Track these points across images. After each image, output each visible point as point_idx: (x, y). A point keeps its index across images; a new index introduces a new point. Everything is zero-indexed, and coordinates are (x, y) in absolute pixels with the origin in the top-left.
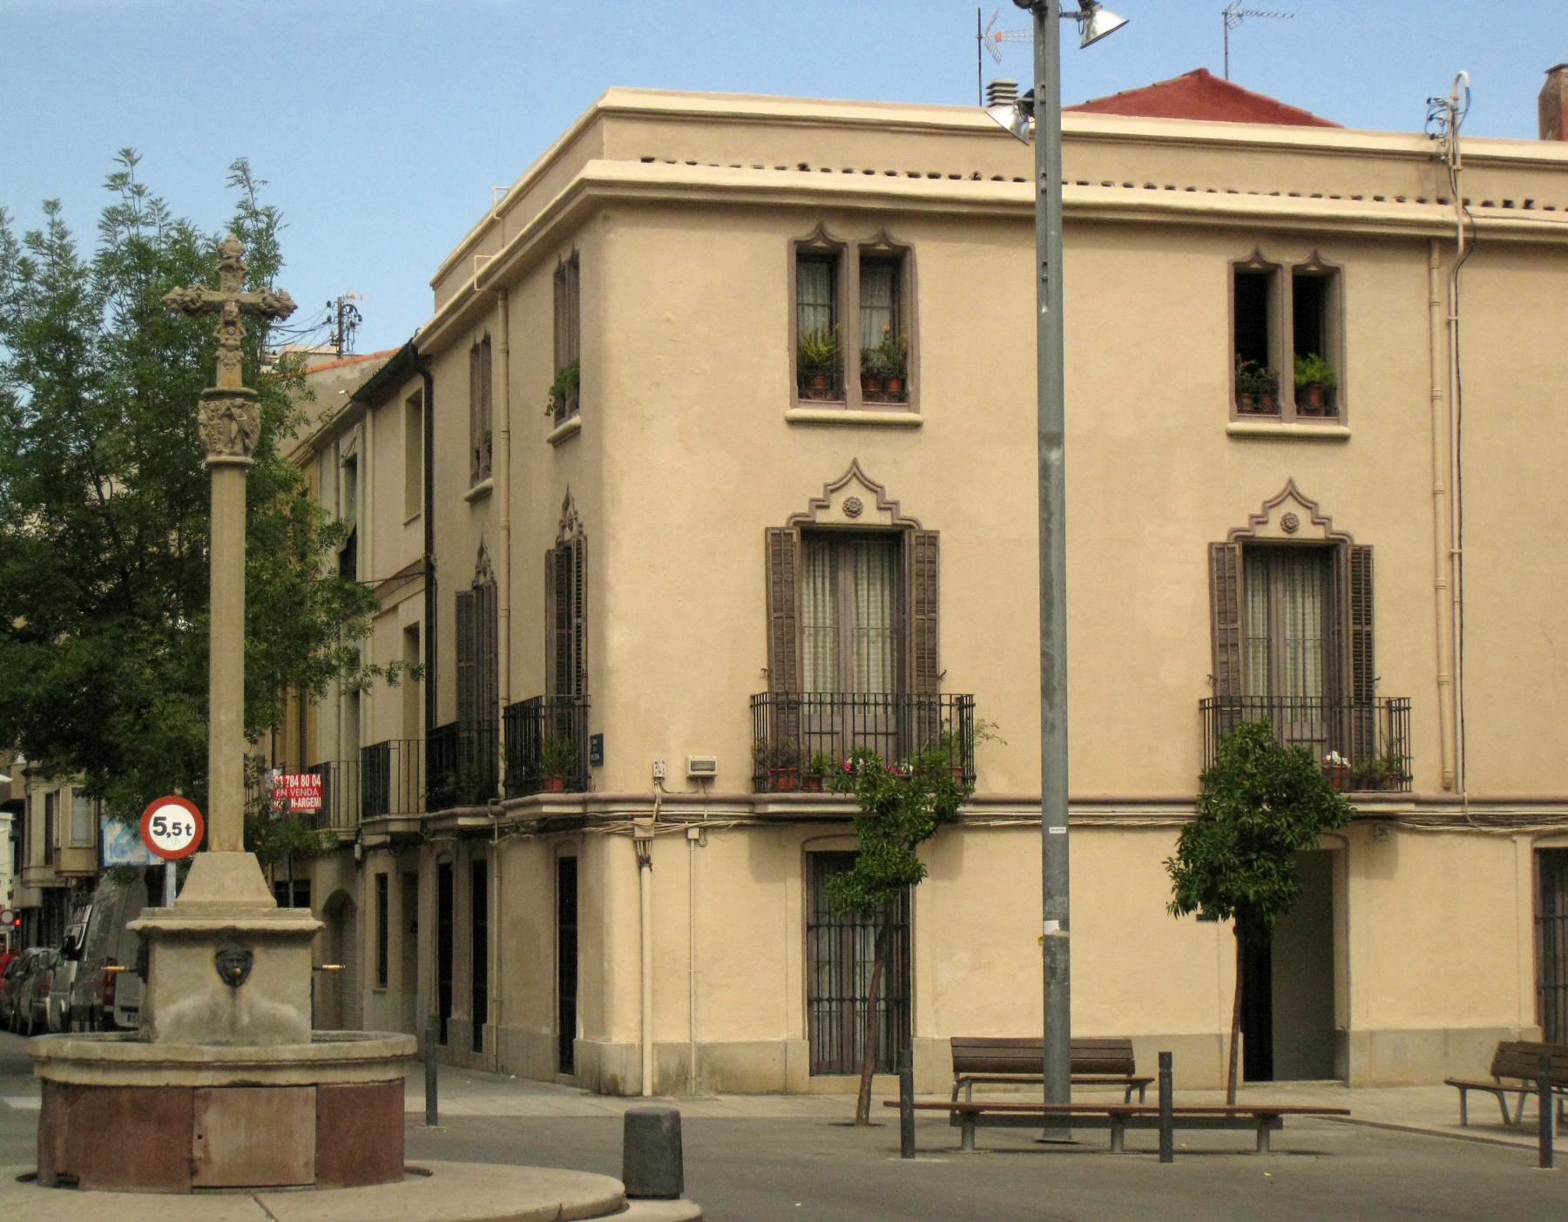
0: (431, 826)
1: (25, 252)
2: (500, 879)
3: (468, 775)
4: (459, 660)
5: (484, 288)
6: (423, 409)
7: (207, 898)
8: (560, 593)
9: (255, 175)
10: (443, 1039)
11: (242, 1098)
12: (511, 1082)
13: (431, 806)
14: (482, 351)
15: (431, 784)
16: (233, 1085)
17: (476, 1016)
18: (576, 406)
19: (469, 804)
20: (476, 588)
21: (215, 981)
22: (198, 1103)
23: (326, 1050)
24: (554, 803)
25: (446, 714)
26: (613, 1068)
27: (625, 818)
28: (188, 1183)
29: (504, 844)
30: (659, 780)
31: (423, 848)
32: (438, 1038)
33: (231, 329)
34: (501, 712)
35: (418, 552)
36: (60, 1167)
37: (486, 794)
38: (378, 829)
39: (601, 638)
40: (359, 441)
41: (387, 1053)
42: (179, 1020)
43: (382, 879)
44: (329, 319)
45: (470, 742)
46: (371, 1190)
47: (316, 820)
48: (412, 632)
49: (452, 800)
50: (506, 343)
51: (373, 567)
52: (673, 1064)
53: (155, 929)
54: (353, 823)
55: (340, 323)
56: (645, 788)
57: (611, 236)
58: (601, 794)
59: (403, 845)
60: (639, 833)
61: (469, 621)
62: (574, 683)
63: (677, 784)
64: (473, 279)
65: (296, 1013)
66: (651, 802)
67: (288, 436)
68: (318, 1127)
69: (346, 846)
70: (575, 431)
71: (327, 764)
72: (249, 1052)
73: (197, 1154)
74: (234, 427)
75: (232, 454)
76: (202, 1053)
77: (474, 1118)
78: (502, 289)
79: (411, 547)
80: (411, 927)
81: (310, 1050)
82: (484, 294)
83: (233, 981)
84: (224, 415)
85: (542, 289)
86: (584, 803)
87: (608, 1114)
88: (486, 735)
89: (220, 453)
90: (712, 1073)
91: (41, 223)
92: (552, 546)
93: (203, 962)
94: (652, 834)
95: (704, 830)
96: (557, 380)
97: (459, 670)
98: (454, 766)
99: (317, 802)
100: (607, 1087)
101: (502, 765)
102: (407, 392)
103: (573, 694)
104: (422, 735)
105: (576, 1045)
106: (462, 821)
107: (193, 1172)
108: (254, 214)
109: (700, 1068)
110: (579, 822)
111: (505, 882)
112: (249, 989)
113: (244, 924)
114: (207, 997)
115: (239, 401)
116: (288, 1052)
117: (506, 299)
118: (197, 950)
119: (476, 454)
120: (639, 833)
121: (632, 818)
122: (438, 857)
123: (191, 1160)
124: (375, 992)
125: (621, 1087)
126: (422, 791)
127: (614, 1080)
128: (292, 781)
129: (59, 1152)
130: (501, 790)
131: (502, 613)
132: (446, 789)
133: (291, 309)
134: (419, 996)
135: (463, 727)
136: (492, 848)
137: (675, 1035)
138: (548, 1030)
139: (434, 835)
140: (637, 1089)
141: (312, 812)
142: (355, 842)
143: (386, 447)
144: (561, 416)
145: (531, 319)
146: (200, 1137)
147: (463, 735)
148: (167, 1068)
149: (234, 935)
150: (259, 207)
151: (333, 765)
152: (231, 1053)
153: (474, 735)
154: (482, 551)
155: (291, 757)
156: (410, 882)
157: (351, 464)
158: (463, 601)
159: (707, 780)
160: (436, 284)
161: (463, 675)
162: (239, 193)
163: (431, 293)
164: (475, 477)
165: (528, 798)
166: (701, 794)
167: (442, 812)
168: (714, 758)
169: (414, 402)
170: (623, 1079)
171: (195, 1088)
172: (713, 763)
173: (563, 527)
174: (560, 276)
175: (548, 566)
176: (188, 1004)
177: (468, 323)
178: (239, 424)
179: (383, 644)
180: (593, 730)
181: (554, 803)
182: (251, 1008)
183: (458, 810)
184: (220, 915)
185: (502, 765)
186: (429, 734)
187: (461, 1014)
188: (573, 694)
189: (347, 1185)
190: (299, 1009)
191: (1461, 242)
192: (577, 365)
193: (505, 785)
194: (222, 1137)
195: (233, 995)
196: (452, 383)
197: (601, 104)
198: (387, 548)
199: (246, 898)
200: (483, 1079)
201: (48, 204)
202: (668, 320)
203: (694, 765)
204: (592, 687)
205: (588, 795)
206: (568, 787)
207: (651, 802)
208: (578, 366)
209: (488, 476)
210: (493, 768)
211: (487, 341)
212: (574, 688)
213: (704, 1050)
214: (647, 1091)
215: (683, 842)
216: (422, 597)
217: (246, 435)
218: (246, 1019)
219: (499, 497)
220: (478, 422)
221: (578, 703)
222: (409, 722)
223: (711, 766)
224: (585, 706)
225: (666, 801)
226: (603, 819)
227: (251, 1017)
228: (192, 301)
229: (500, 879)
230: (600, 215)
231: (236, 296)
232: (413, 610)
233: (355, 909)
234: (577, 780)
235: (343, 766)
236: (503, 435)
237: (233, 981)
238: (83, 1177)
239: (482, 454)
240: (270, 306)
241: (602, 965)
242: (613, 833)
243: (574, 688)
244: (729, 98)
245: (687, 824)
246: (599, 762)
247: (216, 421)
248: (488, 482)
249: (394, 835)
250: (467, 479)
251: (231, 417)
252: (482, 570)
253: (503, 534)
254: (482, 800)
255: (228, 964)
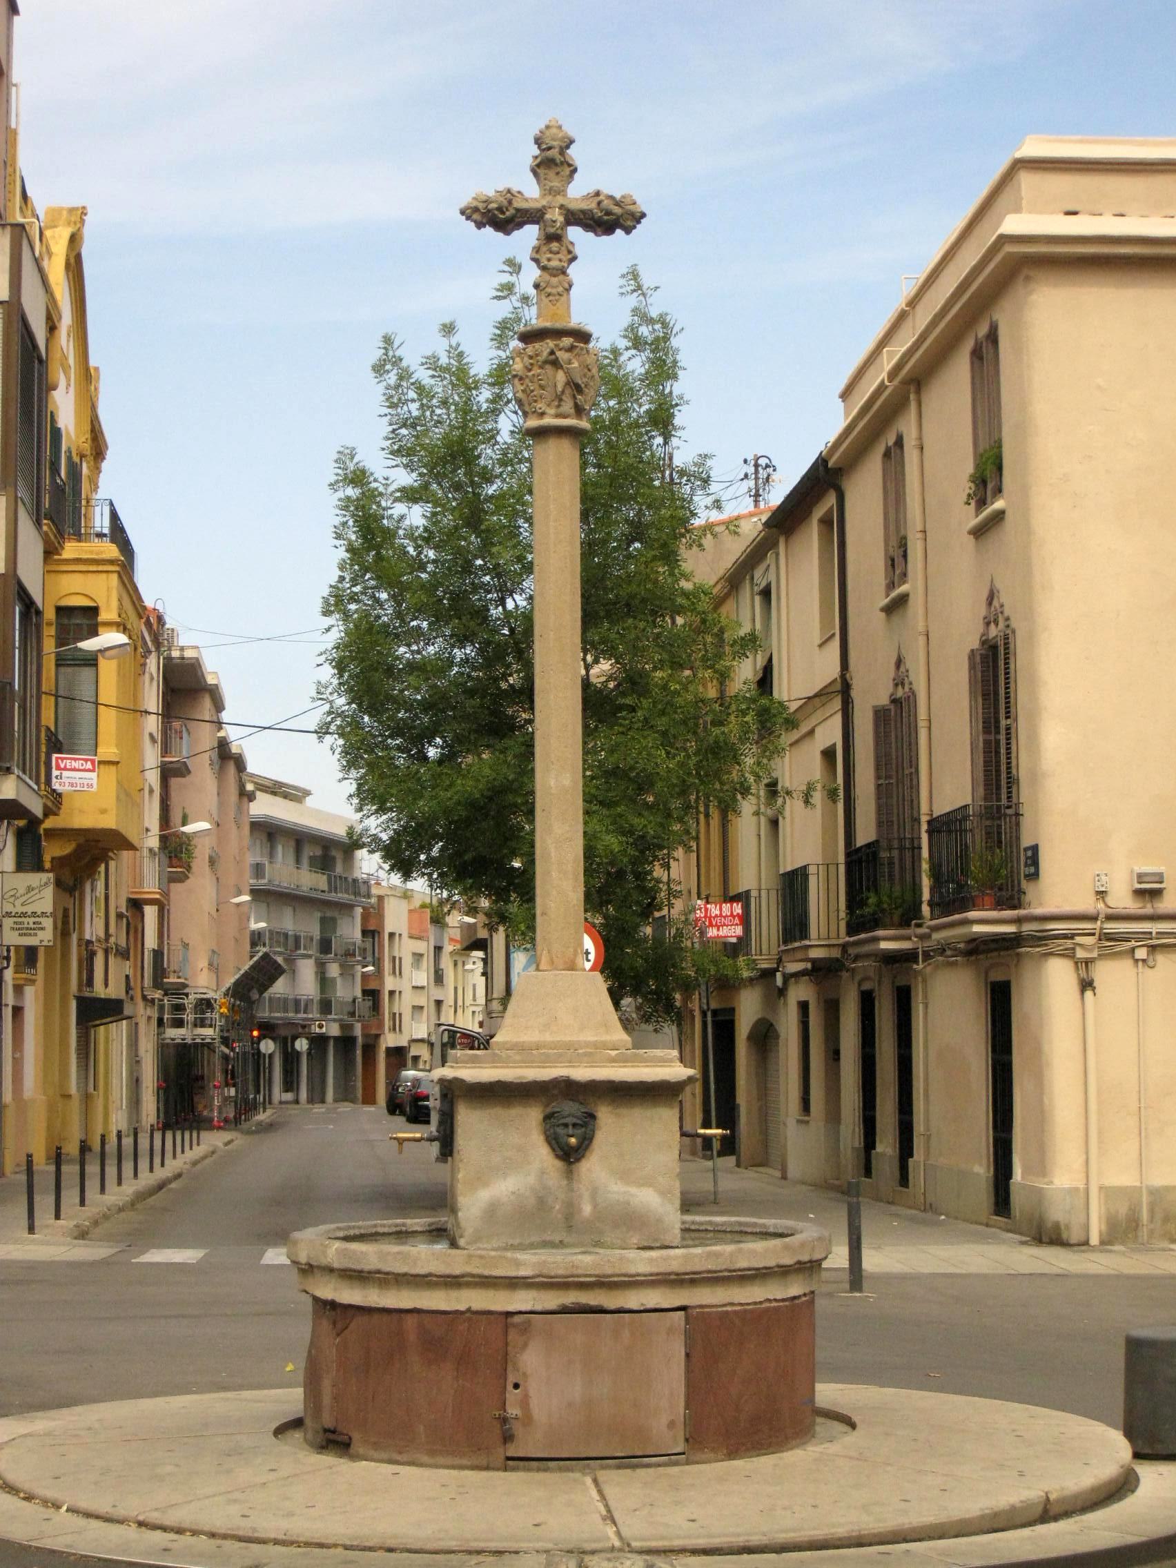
0: (852, 951)
1: (424, 376)
2: (926, 1006)
3: (890, 897)
4: (878, 777)
5: (896, 382)
6: (835, 527)
7: (530, 1037)
8: (985, 696)
9: (647, 282)
10: (868, 1172)
11: (576, 1329)
12: (941, 1223)
13: (852, 929)
14: (894, 455)
15: (851, 906)
16: (564, 1310)
17: (901, 1149)
18: (999, 490)
19: (892, 926)
20: (894, 701)
21: (542, 1154)
22: (513, 1335)
23: (697, 1257)
24: (985, 922)
25: (866, 833)
26: (1056, 1213)
27: (1065, 937)
28: (500, 1453)
29: (929, 969)
30: (1101, 894)
31: (845, 975)
32: (863, 1171)
33: (554, 246)
34: (924, 827)
35: (834, 671)
36: (328, 1421)
37: (909, 916)
38: (799, 955)
39: (1034, 737)
40: (773, 569)
41: (788, 1260)
42: (492, 1211)
43: (804, 1007)
44: (746, 476)
45: (891, 864)
46: (764, 1463)
47: (735, 949)
48: (829, 754)
49: (875, 922)
50: (920, 438)
51: (791, 688)
52: (1123, 1210)
53: (457, 1081)
54: (774, 951)
55: (757, 479)
56: (1084, 903)
57: (1034, 297)
58: (1038, 911)
59: (822, 972)
60: (1080, 954)
61: (887, 735)
62: (1004, 791)
63: (1122, 899)
64: (884, 375)
65: (656, 1199)
66: (1093, 918)
67: (695, 548)
68: (688, 1371)
69: (768, 974)
70: (999, 516)
71: (748, 892)
72: (585, 1262)
73: (513, 1411)
74: (561, 377)
75: (557, 416)
76: (518, 1264)
77: (903, 1278)
78: (914, 381)
79: (827, 667)
80: (834, 1054)
81: (677, 1259)
82: (896, 388)
83: (570, 1155)
84: (546, 362)
85: (960, 371)
86: (1018, 921)
87: (1055, 1271)
88: (908, 854)
89: (542, 414)
90: (1166, 1219)
91: (440, 347)
92: (976, 645)
93: (525, 1128)
94: (1095, 954)
95: (1153, 949)
96: (977, 466)
97: (878, 786)
98: (876, 888)
99: (739, 931)
100: (1048, 1235)
101: (926, 883)
102: (819, 512)
103: (1004, 802)
104: (841, 858)
105: (1012, 1188)
106: (884, 945)
107: (508, 1438)
108: (651, 321)
109: (1152, 1212)
110: (1008, 944)
111: (930, 1010)
112: (593, 1167)
113: (581, 1074)
114: (531, 1180)
115: (567, 341)
116: (642, 1263)
117: (918, 392)
118: (515, 1111)
119: (892, 563)
120: (1080, 954)
121: (1072, 937)
122: (859, 985)
123: (504, 1420)
124: (798, 1121)
125: (1065, 1236)
126: (842, 915)
127: (1057, 1226)
128: (714, 910)
129: (327, 1400)
130: (926, 909)
131: (922, 724)
132: (867, 910)
133: (639, 217)
134: (842, 1127)
135: (884, 844)
136: (916, 972)
137: (1126, 1179)
138: (982, 1170)
139: (854, 961)
140: (1083, 1239)
141: (734, 940)
142: (777, 970)
143: (800, 573)
144: (982, 503)
145: (942, 432)
146: (516, 1386)
147: (884, 854)
148: (468, 1285)
149: (568, 1089)
150: (654, 313)
151: (754, 894)
152: (559, 1261)
153: (895, 853)
154: (899, 662)
155: (715, 888)
156: (832, 1009)
157: (766, 593)
158: (881, 716)
159: (1155, 894)
160: (845, 395)
161: (882, 792)
162: (633, 300)
163: (840, 404)
164: (891, 586)
165: (957, 917)
166: (1148, 910)
167: (863, 936)
168: (1162, 869)
169: (826, 522)
170: (1068, 1227)
171: (509, 1314)
172: (1161, 875)
173: (988, 624)
174: (977, 355)
175: (972, 667)
176: (506, 1188)
177: (879, 425)
178: (567, 373)
179: (799, 766)
180: (1026, 842)
181: (985, 922)
182: (594, 1193)
183: (880, 933)
184: (546, 1061)
185: (926, 883)
186: (848, 855)
187: (886, 1146)
188: (1004, 802)
189: (732, 1454)
190: (663, 1193)
191: (708, 1131)
192: (998, 445)
193: (930, 904)
194: (547, 1387)
195: (569, 1174)
196: (864, 496)
197: (1018, 155)
198: (803, 668)
199: (589, 1036)
200: (912, 1219)
201: (444, 326)
202: (1099, 387)
203: (1141, 877)
204: (1025, 793)
205: (1022, 912)
206: (1000, 904)
207: (1093, 918)
208: (1000, 447)
209: (904, 583)
210: (916, 888)
211: (899, 442)
212: (1004, 796)
213: (1155, 1193)
214: (1094, 1240)
215: (1130, 962)
216: (838, 719)
217: (578, 389)
218: (587, 1209)
219: (916, 605)
220: (892, 527)
221: (1009, 811)
222: (828, 843)
223: (1160, 878)
224: (1018, 815)
225: (1110, 918)
226: (1041, 939)
227: (595, 1206)
228: (500, 209)
229: (926, 1006)
230: (1022, 277)
231: (560, 200)
232: (830, 733)
233: (777, 1037)
234: (1009, 896)
235: (764, 893)
236: (920, 535)
237: (570, 1155)
238: (356, 1436)
239: (897, 562)
240: (608, 213)
241: (1041, 1102)
242: (1051, 954)
243: (1004, 796)
244: (1156, 144)
245: (1133, 944)
246: (1035, 876)
247: (536, 371)
248: (904, 588)
249: (814, 961)
250: (883, 588)
251: (555, 364)
252: (899, 682)
253: (922, 640)
254: (905, 922)
255: (561, 1131)
